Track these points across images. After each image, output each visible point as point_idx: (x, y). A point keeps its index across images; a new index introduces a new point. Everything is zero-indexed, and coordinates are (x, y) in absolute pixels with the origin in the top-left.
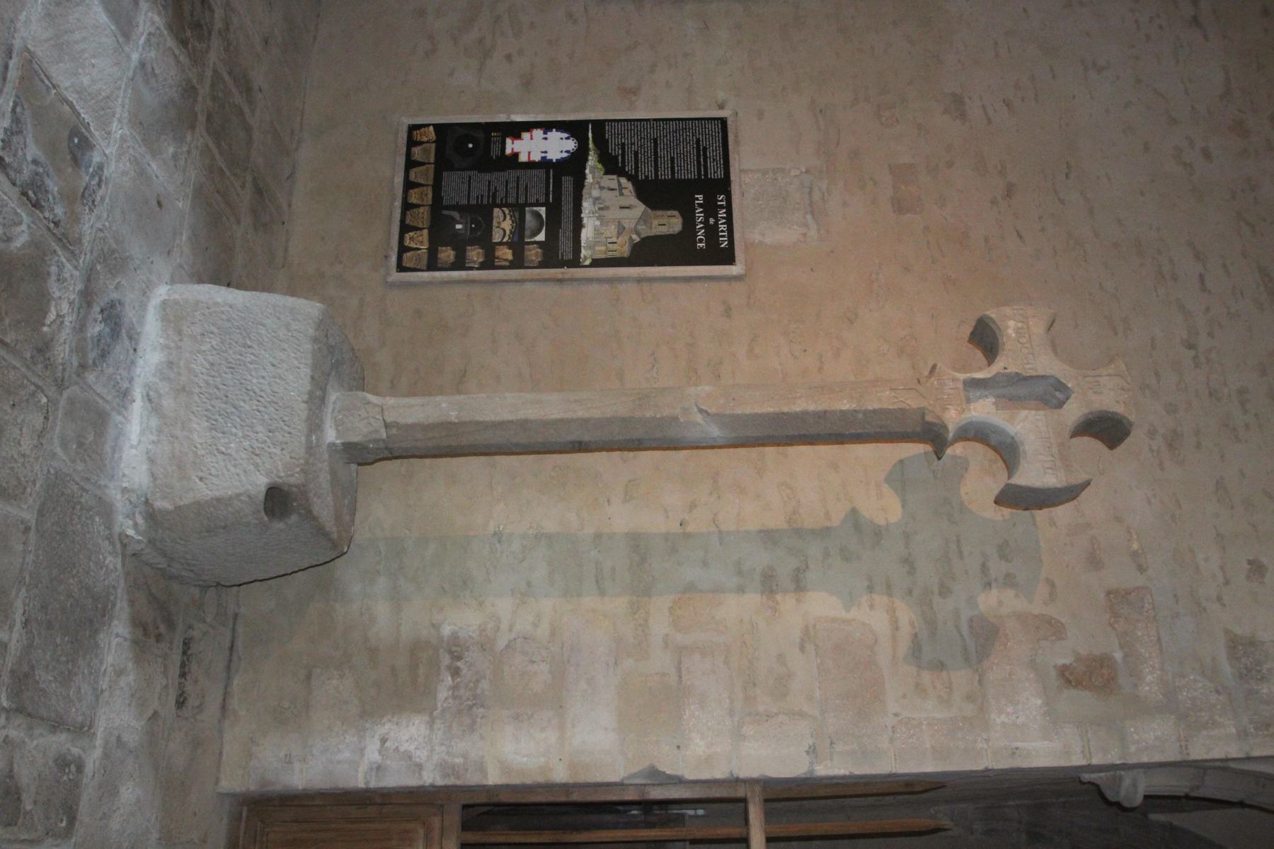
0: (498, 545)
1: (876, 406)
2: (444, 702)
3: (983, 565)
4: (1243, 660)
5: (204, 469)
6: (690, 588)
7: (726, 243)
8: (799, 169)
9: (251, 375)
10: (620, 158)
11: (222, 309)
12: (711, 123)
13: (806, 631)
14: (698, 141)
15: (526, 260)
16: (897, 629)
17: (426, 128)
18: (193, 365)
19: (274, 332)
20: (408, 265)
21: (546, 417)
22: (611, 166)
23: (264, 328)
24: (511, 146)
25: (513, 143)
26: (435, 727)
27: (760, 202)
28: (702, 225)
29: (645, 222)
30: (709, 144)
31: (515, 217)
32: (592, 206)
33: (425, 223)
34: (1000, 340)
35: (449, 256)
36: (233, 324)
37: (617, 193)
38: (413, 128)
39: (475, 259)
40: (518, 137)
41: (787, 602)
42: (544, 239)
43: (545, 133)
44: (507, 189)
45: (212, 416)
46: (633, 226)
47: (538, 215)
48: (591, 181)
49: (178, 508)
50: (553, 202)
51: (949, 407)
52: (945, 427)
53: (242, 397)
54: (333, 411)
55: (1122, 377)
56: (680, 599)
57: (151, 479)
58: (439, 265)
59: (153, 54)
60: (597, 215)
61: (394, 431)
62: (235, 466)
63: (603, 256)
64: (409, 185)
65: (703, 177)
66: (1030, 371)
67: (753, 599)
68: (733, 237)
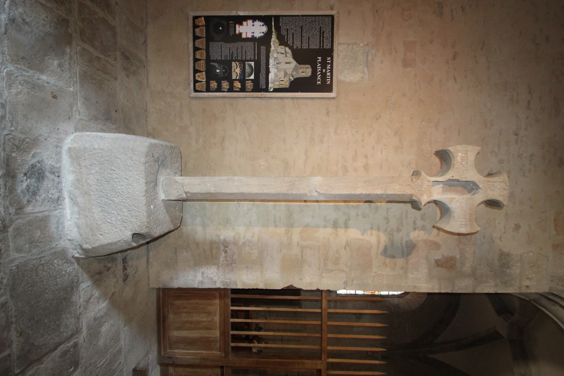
0: (239, 208)
1: (392, 193)
2: (222, 262)
3: (414, 221)
4: (503, 261)
5: (102, 230)
6: (307, 226)
7: (329, 82)
8: (363, 43)
9: (117, 185)
10: (286, 37)
11: (98, 151)
12: (327, 18)
13: (347, 242)
14: (320, 28)
15: (246, 88)
16: (379, 243)
17: (201, 18)
18: (88, 181)
19: (125, 162)
20: (198, 89)
21: (251, 192)
22: (282, 42)
23: (119, 160)
24: (239, 29)
25: (239, 28)
26: (220, 269)
27: (345, 60)
28: (320, 73)
29: (296, 70)
30: (325, 30)
31: (241, 67)
32: (274, 62)
33: (204, 68)
34: (452, 162)
35: (214, 85)
36: (104, 159)
37: (284, 55)
38: (195, 18)
39: (226, 87)
40: (241, 24)
41: (341, 231)
42: (253, 78)
43: (253, 22)
44: (237, 52)
45: (102, 206)
46: (291, 72)
47: (251, 66)
48: (273, 49)
49: (93, 248)
50: (257, 60)
51: (424, 194)
52: (421, 203)
53: (114, 196)
54: (162, 185)
55: (505, 183)
56: (303, 229)
57: (80, 235)
58: (211, 90)
59: (21, 10)
60: (276, 66)
61: (189, 195)
62: (115, 228)
63: (278, 87)
64: (196, 49)
65: (322, 48)
66: (463, 179)
67: (329, 230)
68: (332, 79)
